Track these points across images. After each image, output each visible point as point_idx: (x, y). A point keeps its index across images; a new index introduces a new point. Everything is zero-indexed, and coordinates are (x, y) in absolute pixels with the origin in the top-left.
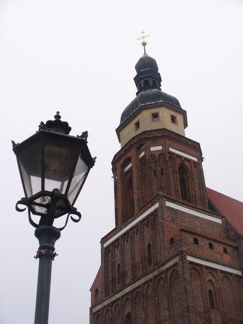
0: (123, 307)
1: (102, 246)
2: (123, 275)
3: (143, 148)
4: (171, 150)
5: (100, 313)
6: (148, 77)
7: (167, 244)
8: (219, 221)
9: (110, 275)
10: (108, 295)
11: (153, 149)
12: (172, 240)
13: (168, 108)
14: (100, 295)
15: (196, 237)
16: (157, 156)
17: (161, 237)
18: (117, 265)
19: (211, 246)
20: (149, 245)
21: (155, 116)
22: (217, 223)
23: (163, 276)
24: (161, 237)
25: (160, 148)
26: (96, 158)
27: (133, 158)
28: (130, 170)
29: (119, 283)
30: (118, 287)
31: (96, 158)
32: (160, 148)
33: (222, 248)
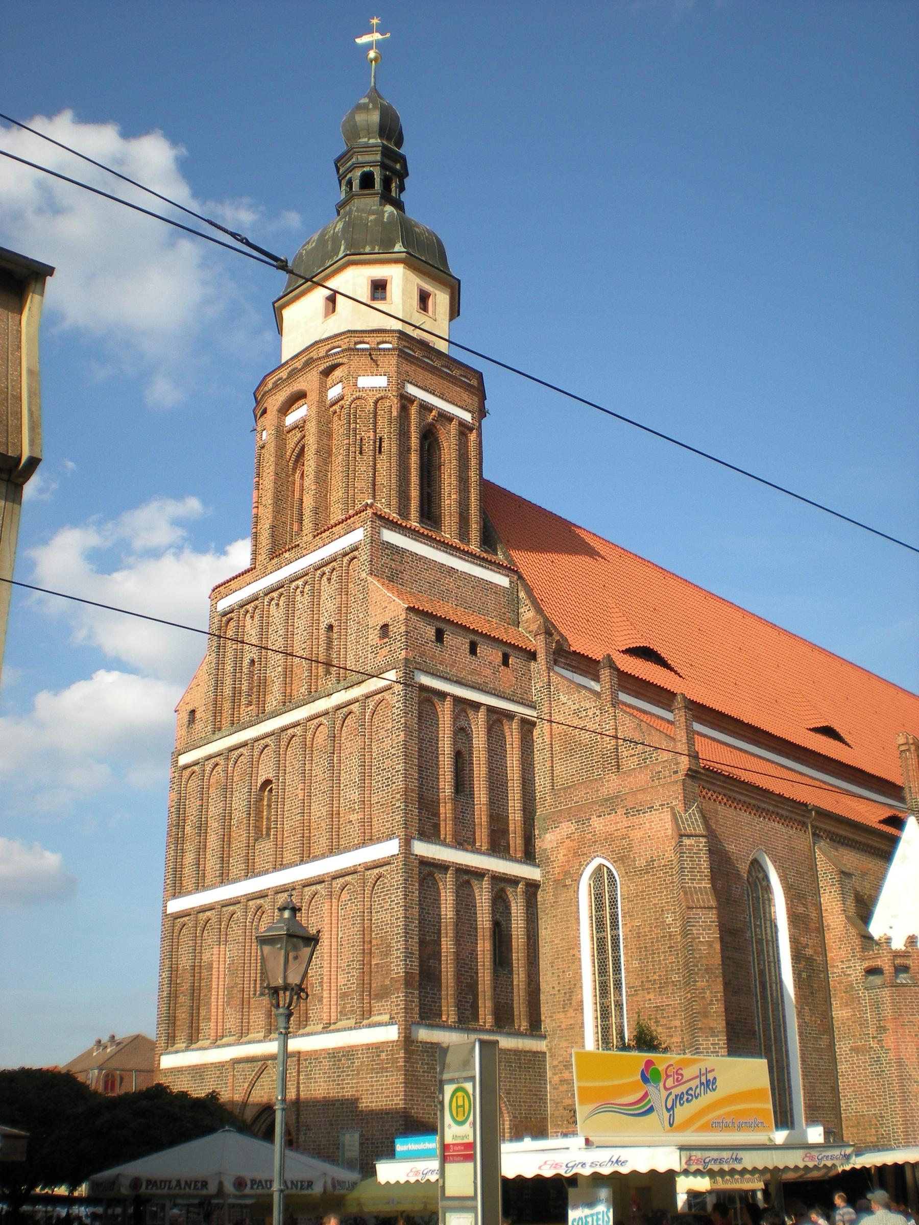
0: (253, 764)
1: (214, 606)
2: (262, 686)
3: (338, 373)
4: (412, 390)
5: (195, 768)
6: (371, 164)
7: (374, 637)
8: (502, 581)
9: (228, 681)
10: (220, 729)
11: (365, 382)
12: (385, 627)
13: (440, 283)
14: (199, 726)
15: (475, 638)
16: (371, 402)
17: (361, 616)
18: (246, 662)
19: (473, 650)
20: (330, 628)
21: (379, 288)
22: (496, 585)
23: (355, 707)
24: (361, 616)
25: (381, 381)
26: (319, 932)
27: (313, 396)
28: (300, 426)
29: (250, 704)
30: (246, 712)
31: (319, 932)
32: (381, 381)
33: (500, 654)
